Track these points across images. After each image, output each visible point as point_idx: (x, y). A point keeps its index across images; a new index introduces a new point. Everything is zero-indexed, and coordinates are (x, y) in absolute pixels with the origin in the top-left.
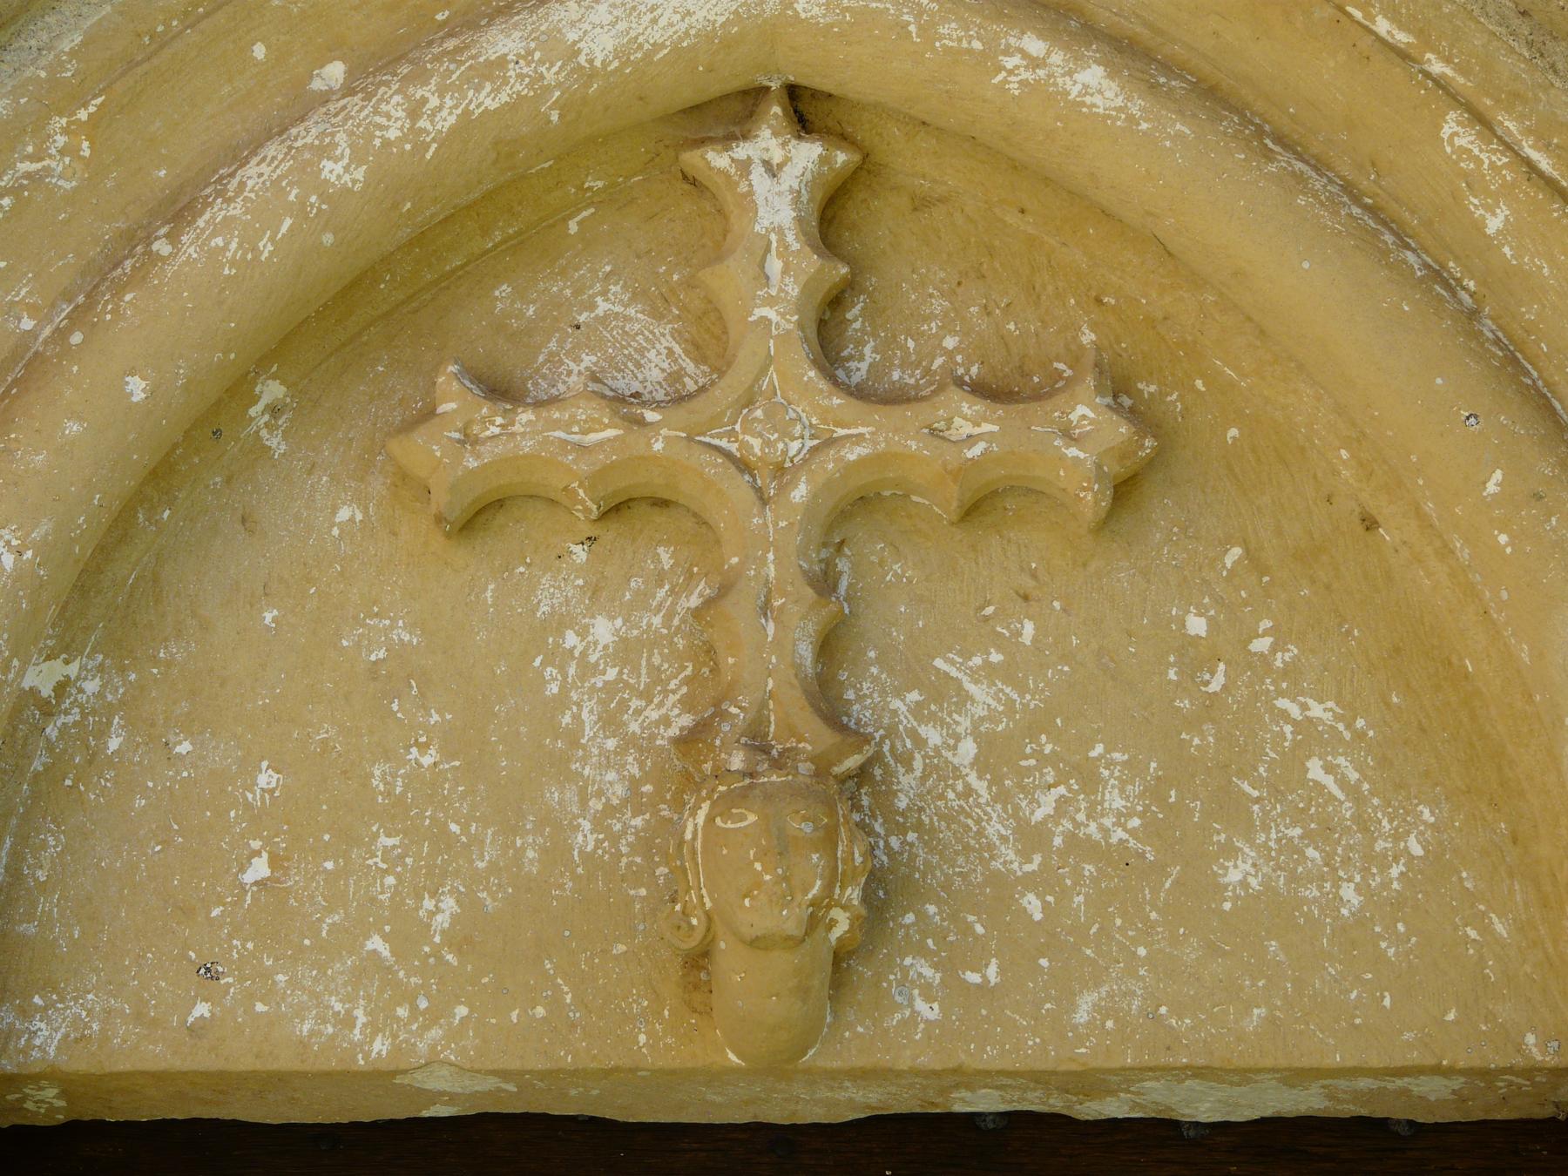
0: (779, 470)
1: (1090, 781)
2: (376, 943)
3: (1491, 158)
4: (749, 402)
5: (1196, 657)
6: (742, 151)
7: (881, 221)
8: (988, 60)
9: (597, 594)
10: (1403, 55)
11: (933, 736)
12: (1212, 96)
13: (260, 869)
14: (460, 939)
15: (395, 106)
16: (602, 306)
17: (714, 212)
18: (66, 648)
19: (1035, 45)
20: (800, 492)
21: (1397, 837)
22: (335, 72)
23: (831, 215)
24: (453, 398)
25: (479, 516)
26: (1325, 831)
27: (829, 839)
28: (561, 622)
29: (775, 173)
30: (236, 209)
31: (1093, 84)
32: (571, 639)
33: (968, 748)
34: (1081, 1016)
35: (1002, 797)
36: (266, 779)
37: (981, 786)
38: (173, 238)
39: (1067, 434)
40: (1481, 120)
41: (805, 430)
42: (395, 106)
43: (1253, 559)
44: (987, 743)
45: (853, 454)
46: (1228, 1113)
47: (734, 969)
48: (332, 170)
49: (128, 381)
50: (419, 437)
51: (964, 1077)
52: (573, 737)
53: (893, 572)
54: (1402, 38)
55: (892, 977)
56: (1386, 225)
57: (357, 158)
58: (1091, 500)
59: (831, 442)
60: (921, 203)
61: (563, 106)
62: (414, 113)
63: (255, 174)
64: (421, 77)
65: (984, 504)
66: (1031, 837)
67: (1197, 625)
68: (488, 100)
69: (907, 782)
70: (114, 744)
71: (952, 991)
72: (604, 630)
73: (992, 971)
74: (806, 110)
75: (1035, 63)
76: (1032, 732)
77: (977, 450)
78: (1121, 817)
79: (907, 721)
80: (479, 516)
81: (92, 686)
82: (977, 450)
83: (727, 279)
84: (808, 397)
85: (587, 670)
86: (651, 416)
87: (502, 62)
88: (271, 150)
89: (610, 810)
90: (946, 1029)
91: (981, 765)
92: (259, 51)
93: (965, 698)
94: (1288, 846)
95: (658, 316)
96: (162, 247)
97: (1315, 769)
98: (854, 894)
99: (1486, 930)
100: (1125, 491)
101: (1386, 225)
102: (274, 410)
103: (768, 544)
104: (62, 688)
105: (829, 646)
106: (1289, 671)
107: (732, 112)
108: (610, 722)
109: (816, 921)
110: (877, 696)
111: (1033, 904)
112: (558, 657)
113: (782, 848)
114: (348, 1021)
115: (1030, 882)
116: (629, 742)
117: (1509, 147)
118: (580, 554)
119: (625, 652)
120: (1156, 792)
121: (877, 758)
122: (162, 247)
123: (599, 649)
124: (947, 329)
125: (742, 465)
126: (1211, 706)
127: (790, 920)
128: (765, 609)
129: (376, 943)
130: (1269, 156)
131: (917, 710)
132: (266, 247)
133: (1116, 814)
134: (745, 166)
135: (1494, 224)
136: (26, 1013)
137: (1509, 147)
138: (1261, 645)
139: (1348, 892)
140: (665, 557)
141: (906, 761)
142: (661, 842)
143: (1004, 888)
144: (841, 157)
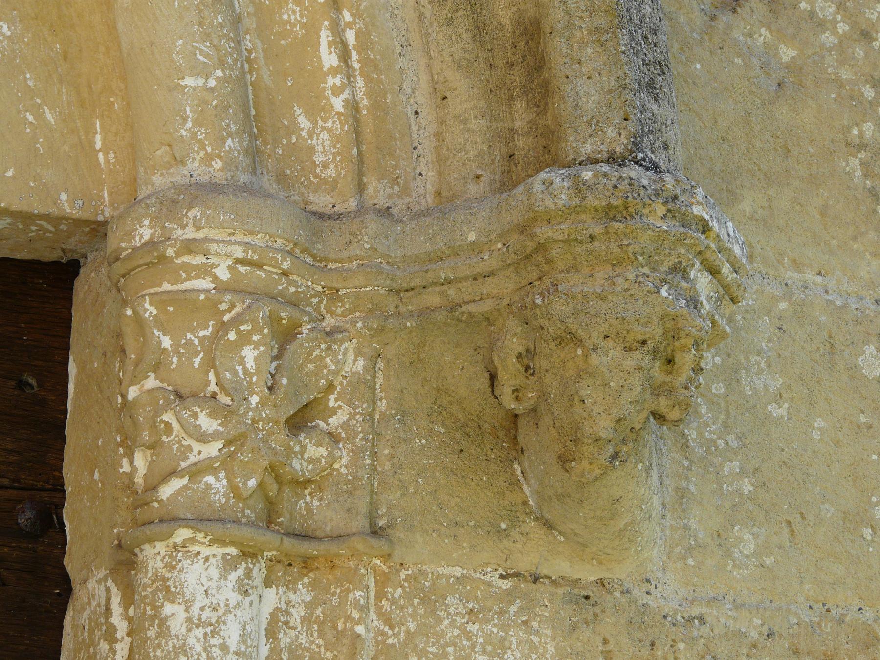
99: (40, 116)
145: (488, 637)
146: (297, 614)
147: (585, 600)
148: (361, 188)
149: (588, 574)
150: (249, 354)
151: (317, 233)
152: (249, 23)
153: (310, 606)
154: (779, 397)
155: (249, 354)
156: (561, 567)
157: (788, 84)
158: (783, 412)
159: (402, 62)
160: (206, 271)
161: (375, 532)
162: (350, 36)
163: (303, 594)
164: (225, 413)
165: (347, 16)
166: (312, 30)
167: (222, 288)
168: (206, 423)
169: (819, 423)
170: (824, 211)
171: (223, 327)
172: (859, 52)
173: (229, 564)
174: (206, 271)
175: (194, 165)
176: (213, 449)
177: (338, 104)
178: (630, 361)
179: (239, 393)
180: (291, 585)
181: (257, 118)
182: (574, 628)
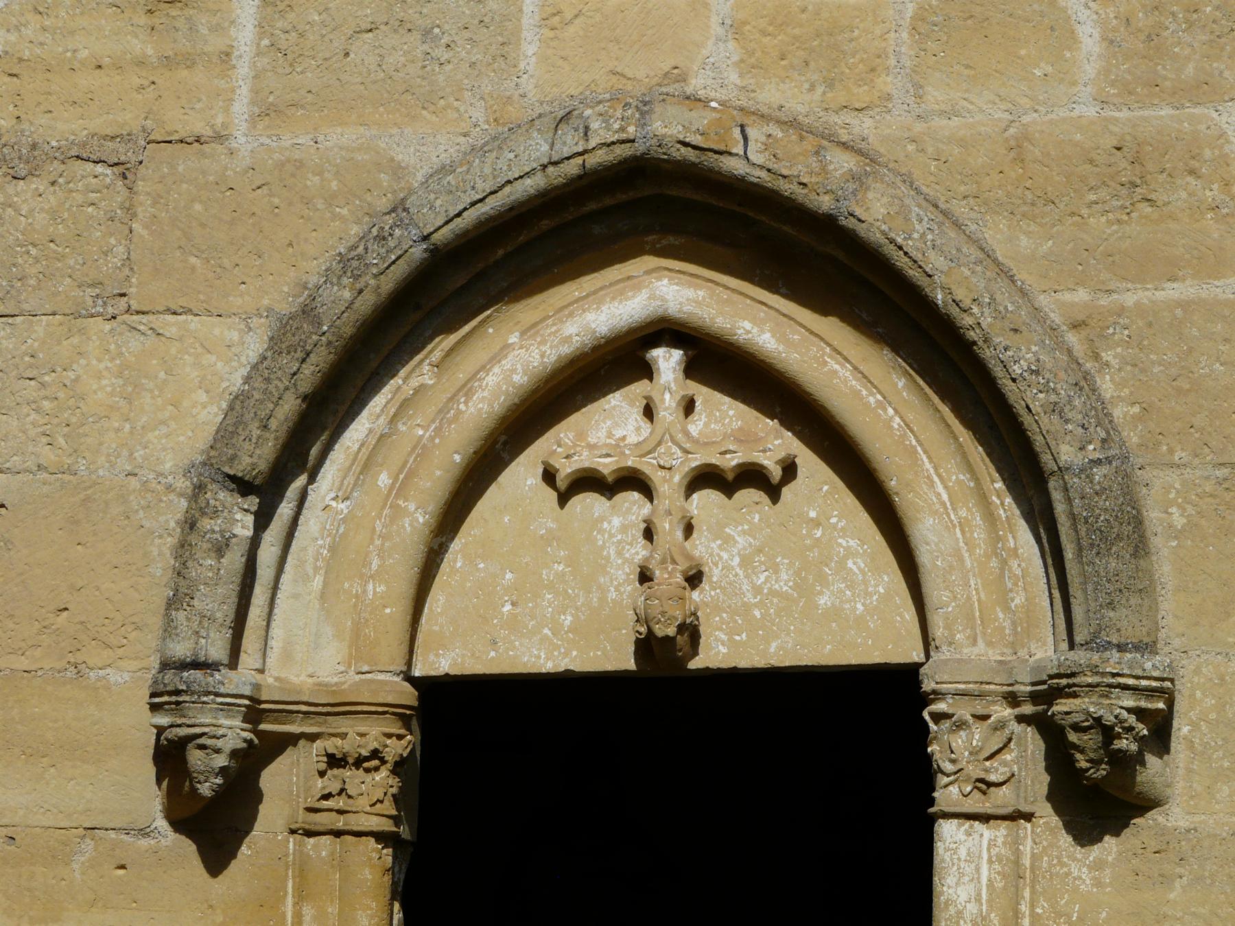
1: (776, 572)
2: (546, 631)
11: (725, 555)
21: (877, 586)
28: (602, 519)
32: (606, 525)
33: (737, 560)
34: (772, 650)
35: (747, 577)
36: (509, 576)
37: (741, 573)
38: (466, 403)
52: (607, 558)
66: (757, 590)
72: (616, 521)
79: (716, 551)
85: (611, 536)
89: (619, 585)
94: (841, 591)
97: (850, 564)
108: (619, 553)
111: (757, 613)
114: (539, 657)
116: (626, 561)
119: (624, 529)
120: (797, 573)
129: (546, 631)
131: (720, 547)
141: (716, 565)
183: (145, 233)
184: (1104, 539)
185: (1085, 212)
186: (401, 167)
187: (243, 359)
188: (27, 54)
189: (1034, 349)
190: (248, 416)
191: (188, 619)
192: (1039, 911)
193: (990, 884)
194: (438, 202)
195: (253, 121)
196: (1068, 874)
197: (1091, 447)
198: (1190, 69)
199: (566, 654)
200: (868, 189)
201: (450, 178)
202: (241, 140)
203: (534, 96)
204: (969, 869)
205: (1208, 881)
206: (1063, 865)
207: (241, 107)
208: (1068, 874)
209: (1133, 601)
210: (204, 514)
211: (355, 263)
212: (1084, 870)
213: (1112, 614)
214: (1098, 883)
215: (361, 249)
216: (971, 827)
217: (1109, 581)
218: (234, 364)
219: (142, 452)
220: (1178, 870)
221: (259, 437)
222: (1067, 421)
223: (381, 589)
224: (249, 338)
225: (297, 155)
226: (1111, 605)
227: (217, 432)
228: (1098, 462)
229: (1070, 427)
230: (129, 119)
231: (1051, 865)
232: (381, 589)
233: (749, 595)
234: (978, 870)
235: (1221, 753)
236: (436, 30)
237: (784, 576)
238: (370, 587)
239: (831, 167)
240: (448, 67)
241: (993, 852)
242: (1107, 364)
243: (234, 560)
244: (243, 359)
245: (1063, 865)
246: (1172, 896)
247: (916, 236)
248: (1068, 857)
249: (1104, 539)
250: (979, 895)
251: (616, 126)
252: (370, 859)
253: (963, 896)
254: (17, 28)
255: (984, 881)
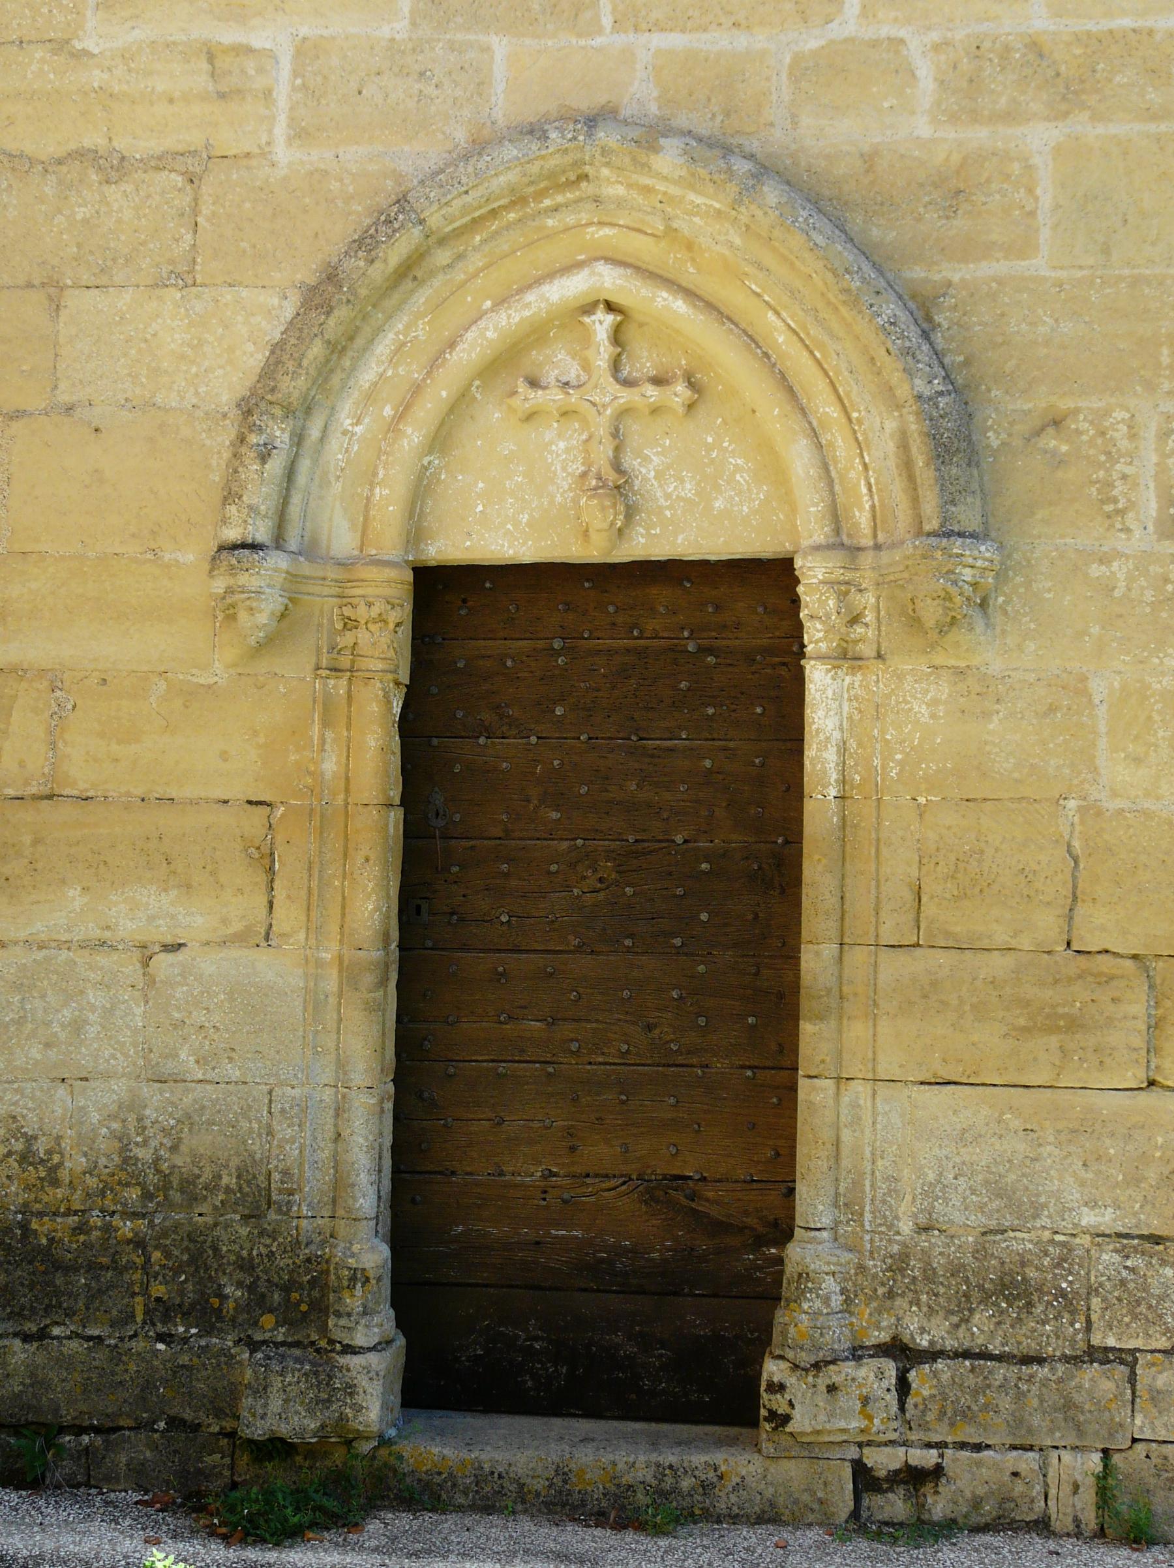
0: (604, 406)
1: (682, 481)
2: (509, 526)
3: (780, 324)
4: (596, 387)
5: (709, 448)
6: (593, 318)
7: (631, 333)
8: (653, 299)
9: (560, 436)
10: (758, 295)
11: (644, 471)
12: (710, 306)
13: (480, 508)
14: (529, 524)
15: (504, 316)
16: (560, 357)
17: (586, 338)
18: (430, 453)
19: (665, 294)
20: (609, 412)
21: (757, 494)
22: (488, 303)
23: (617, 337)
24: (522, 387)
25: (529, 417)
26: (739, 493)
27: (614, 506)
28: (551, 443)
29: (602, 323)
30: (466, 346)
31: (680, 305)
32: (554, 447)
33: (653, 473)
34: (679, 541)
35: (661, 486)
36: (481, 485)
37: (655, 483)
38: (450, 353)
39: (675, 395)
40: (777, 313)
41: (611, 394)
42: (504, 316)
43: (725, 422)
44: (657, 472)
45: (622, 401)
46: (339, 665)
47: (594, 536)
48: (489, 334)
49: (441, 392)
50: (514, 398)
51: (650, 555)
52: (555, 473)
53: (634, 429)
54: (758, 290)
55: (128, 1223)
56: (752, 341)
57: (495, 331)
58: (681, 411)
59: (616, 398)
60: (641, 325)
61: (547, 313)
62: (509, 317)
63: (470, 335)
64: (510, 308)
65: (655, 411)
66: (668, 496)
67: (710, 440)
68: (527, 313)
69: (637, 482)
70: (443, 477)
71: (648, 535)
72: (562, 445)
73: (658, 531)
74: (610, 307)
75: (665, 300)
76: (668, 469)
77: (652, 400)
78: (690, 490)
79: (637, 467)
80: (529, 417)
81: (437, 462)
82: (652, 400)
83: (590, 353)
84: (614, 387)
85: (558, 455)
86: (571, 392)
87: (530, 303)
88: (474, 328)
89: (565, 491)
90: (647, 543)
91: (655, 478)
92: (469, 299)
93: (651, 461)
94: (732, 497)
95: (574, 359)
96: (447, 356)
97: (738, 477)
98: (621, 517)
99: (778, 517)
100: (690, 407)
101: (752, 341)
102: (477, 388)
103: (601, 426)
104: (429, 463)
105: (617, 449)
106: (733, 451)
107: (589, 309)
108: (564, 469)
109: (612, 524)
110: (630, 461)
111: (668, 513)
112: (551, 452)
113: (603, 509)
114: (503, 546)
115: (667, 508)
116: (569, 474)
117: (784, 321)
118: (555, 425)
119: (568, 450)
120: (698, 484)
121: (630, 477)
122: (447, 356)
123: (563, 453)
124: (648, 361)
125: (594, 404)
126: (713, 461)
127: (605, 525)
128: (600, 443)
129: (509, 526)
130: (724, 324)
131: (640, 464)
132: (473, 355)
133: (689, 490)
134: (594, 322)
135: (781, 340)
136: (427, 545)
137: (784, 321)
138: (726, 444)
139: (745, 508)
140: (577, 425)
141: (637, 477)
142: (575, 501)
143: (661, 508)
144: (619, 318)
145: (922, 688)
146: (857, 684)
147: (960, 673)
148: (875, 536)
149: (963, 664)
150: (831, 603)
151: (853, 559)
152: (836, 481)
153: (861, 681)
154: (1049, 591)
155: (831, 603)
156: (952, 662)
157: (1060, 462)
158: (1051, 596)
159: (891, 487)
160: (815, 576)
161: (879, 656)
162: (872, 481)
163: (859, 677)
164: (823, 623)
165: (871, 473)
166: (859, 480)
167: (821, 582)
168: (819, 626)
169: (1068, 598)
170: (1077, 512)
171: (822, 594)
172: (1099, 441)
173: (828, 671)
174: (815, 576)
175: (815, 538)
176: (821, 634)
177: (867, 506)
178: (936, 602)
179: (828, 616)
180: (854, 675)
181: (836, 516)
182: (956, 683)
183: (205, 224)
184: (947, 451)
185: (921, 210)
186: (401, 175)
187: (282, 319)
188: (116, 89)
189: (892, 306)
190: (285, 358)
191: (239, 511)
192: (889, 737)
193: (850, 718)
194: (432, 195)
195: (290, 140)
196: (910, 710)
197: (936, 382)
198: (1003, 100)
199: (524, 544)
200: (763, 185)
201: (441, 176)
202: (283, 153)
203: (501, 122)
204: (835, 705)
205: (1019, 716)
206: (907, 702)
207: (280, 130)
208: (910, 710)
209: (969, 500)
210: (251, 431)
211: (369, 241)
212: (924, 706)
213: (953, 509)
214: (933, 716)
215: (372, 231)
216: (836, 673)
217: (951, 484)
218: (276, 323)
219: (205, 389)
220: (997, 707)
221: (294, 372)
222: (918, 362)
223: (386, 492)
224: (285, 303)
225: (322, 166)
226: (953, 502)
227: (263, 369)
228: (941, 393)
229: (920, 366)
230: (194, 138)
231: (898, 703)
232: (386, 492)
233: (662, 500)
234: (840, 706)
235: (1028, 619)
236: (428, 73)
237: (688, 486)
238: (377, 490)
239: (735, 168)
240: (437, 101)
241: (852, 693)
242: (939, 325)
243: (276, 465)
244: (282, 319)
245: (907, 702)
246: (991, 727)
247: (801, 219)
248: (911, 696)
249: (947, 451)
250: (841, 725)
251: (570, 136)
252: (377, 696)
253: (830, 726)
254: (110, 70)
255: (845, 715)
